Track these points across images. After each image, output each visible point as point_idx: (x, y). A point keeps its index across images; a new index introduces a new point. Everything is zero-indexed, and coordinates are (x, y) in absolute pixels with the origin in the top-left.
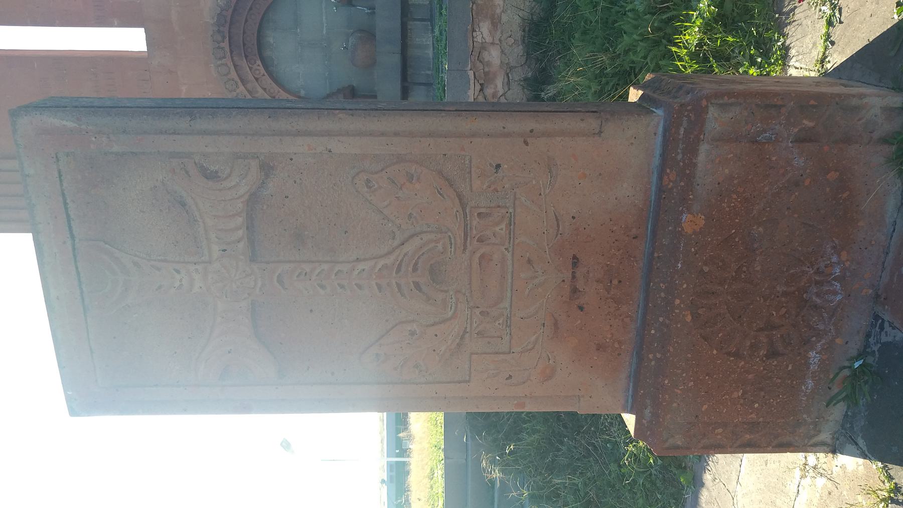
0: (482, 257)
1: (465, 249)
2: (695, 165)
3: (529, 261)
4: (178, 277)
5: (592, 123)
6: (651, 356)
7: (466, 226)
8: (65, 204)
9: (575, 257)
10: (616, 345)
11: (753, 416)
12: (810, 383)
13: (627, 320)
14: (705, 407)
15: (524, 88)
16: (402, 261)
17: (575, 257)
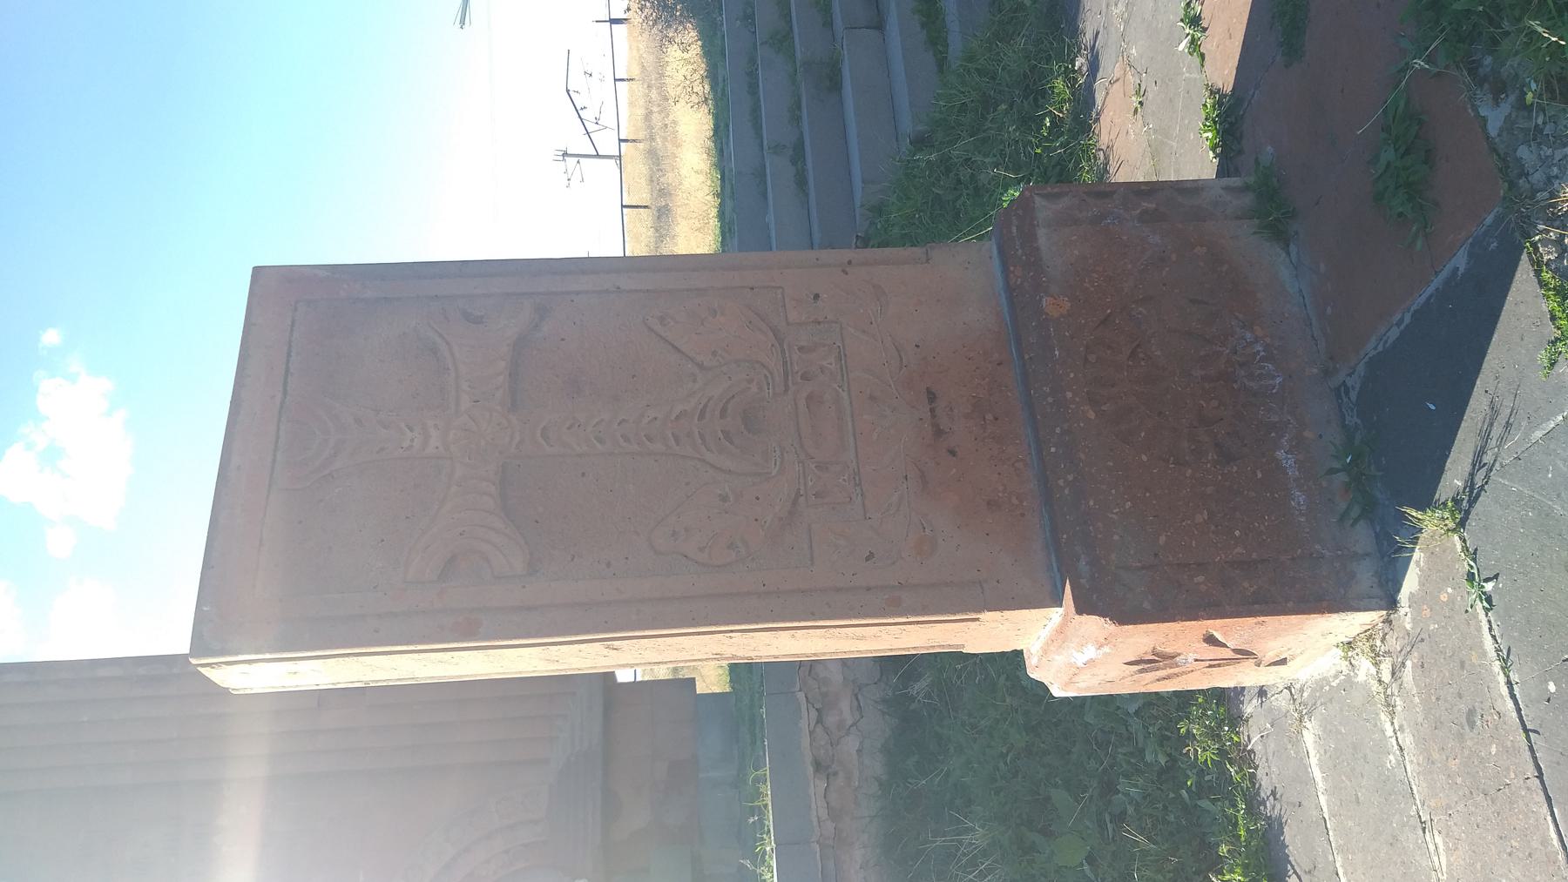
0: (810, 398)
1: (786, 390)
2: (1038, 249)
3: (872, 398)
4: (409, 434)
5: (918, 251)
6: (1061, 482)
7: (785, 363)
8: (289, 355)
9: (929, 391)
10: (1015, 501)
11: (1239, 550)
12: (1299, 498)
13: (1020, 465)
14: (1162, 540)
15: (884, 713)
16: (706, 406)
17: (929, 391)
